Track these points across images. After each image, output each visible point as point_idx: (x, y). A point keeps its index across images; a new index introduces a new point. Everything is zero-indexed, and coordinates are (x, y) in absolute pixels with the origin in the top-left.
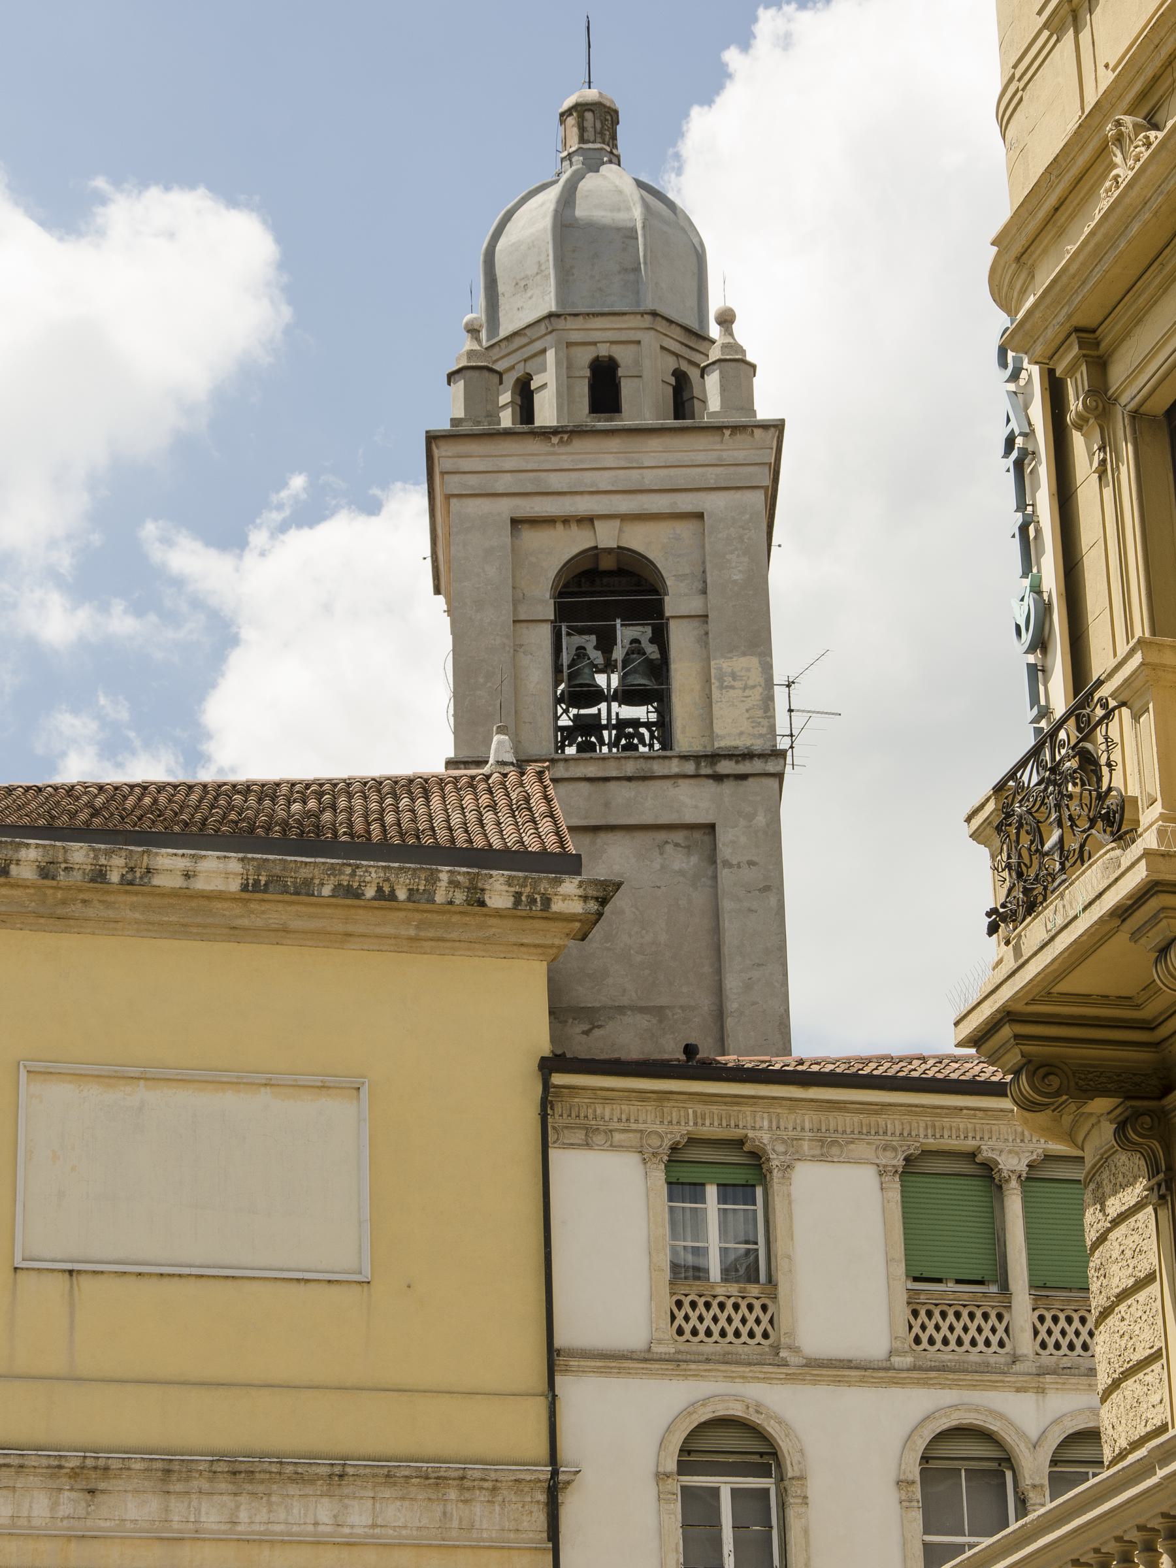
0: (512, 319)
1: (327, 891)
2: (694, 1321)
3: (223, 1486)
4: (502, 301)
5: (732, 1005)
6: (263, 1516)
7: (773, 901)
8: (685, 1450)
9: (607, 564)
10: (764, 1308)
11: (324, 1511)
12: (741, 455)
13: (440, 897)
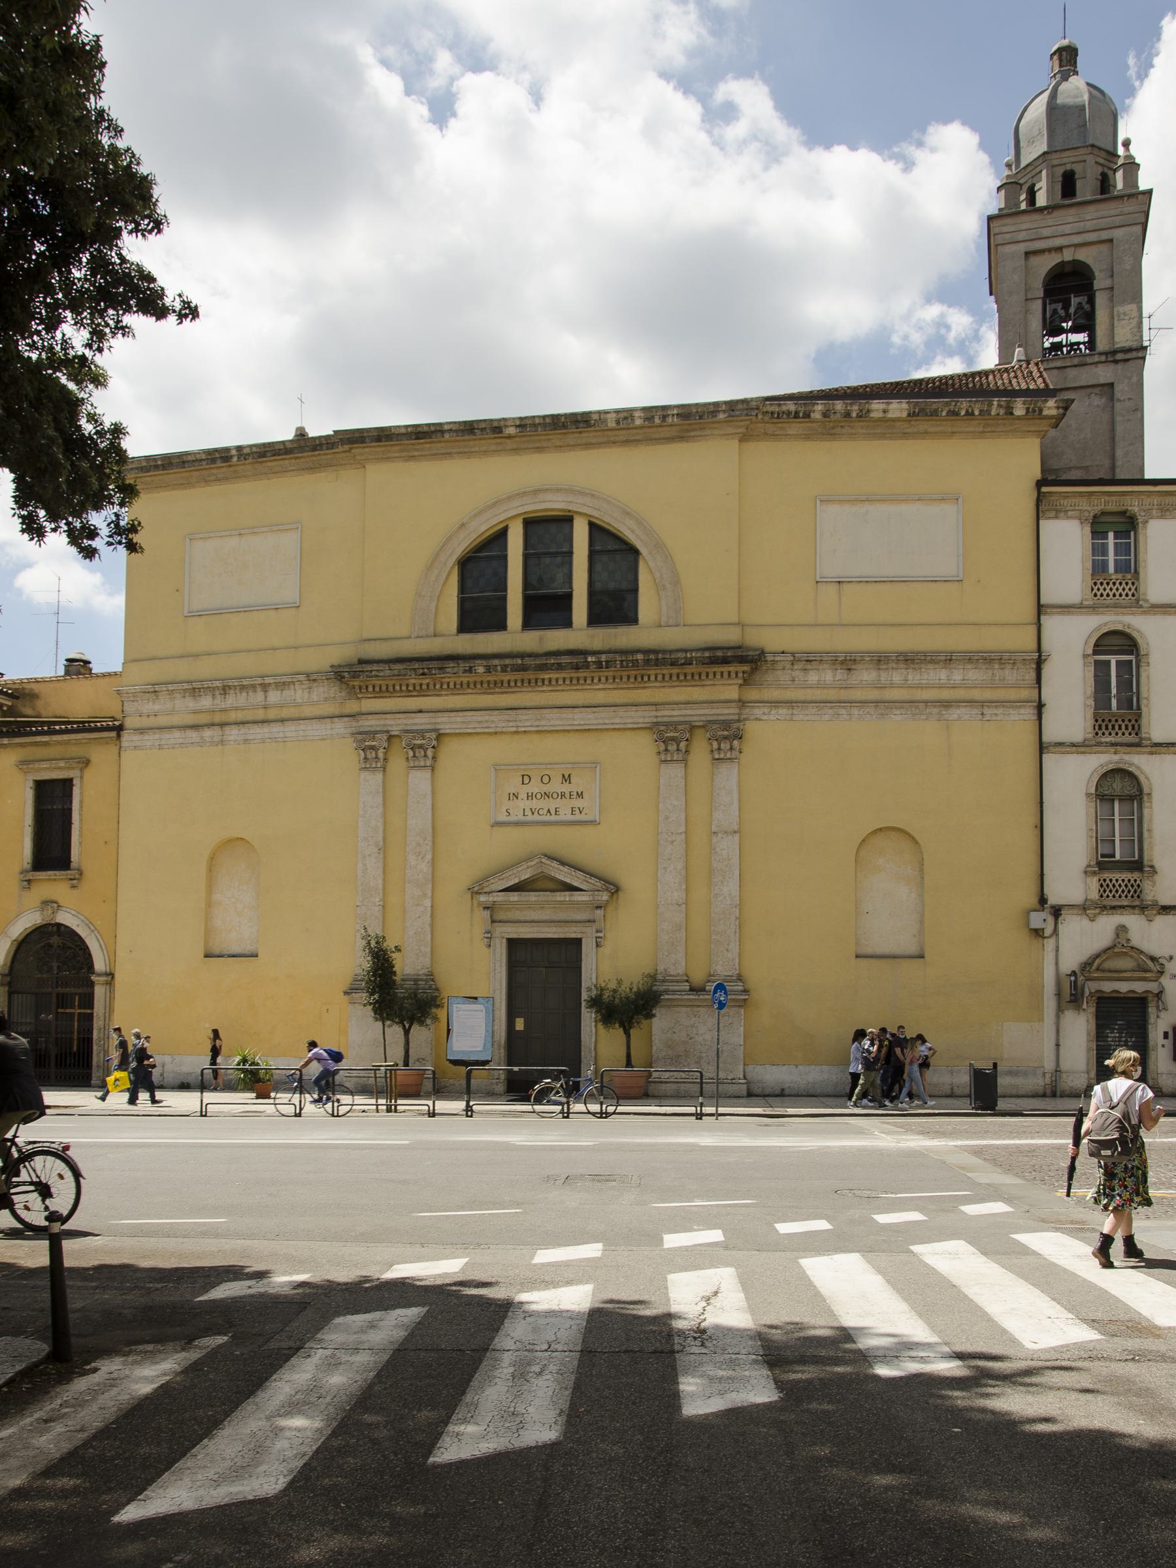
0: (1027, 158)
1: (944, 414)
2: (1101, 591)
3: (902, 666)
4: (1022, 151)
5: (1119, 463)
6: (918, 677)
7: (1139, 415)
8: (1096, 645)
9: (1068, 269)
10: (1133, 584)
11: (943, 675)
12: (1131, 209)
13: (993, 412)
